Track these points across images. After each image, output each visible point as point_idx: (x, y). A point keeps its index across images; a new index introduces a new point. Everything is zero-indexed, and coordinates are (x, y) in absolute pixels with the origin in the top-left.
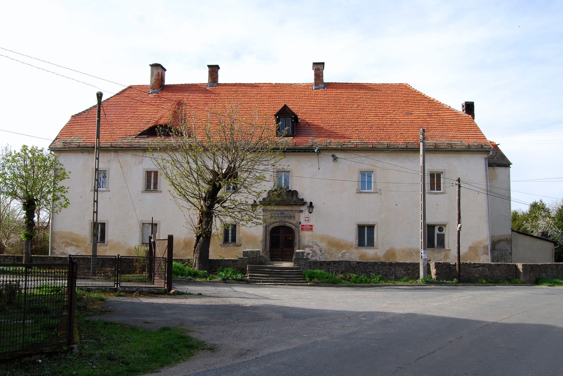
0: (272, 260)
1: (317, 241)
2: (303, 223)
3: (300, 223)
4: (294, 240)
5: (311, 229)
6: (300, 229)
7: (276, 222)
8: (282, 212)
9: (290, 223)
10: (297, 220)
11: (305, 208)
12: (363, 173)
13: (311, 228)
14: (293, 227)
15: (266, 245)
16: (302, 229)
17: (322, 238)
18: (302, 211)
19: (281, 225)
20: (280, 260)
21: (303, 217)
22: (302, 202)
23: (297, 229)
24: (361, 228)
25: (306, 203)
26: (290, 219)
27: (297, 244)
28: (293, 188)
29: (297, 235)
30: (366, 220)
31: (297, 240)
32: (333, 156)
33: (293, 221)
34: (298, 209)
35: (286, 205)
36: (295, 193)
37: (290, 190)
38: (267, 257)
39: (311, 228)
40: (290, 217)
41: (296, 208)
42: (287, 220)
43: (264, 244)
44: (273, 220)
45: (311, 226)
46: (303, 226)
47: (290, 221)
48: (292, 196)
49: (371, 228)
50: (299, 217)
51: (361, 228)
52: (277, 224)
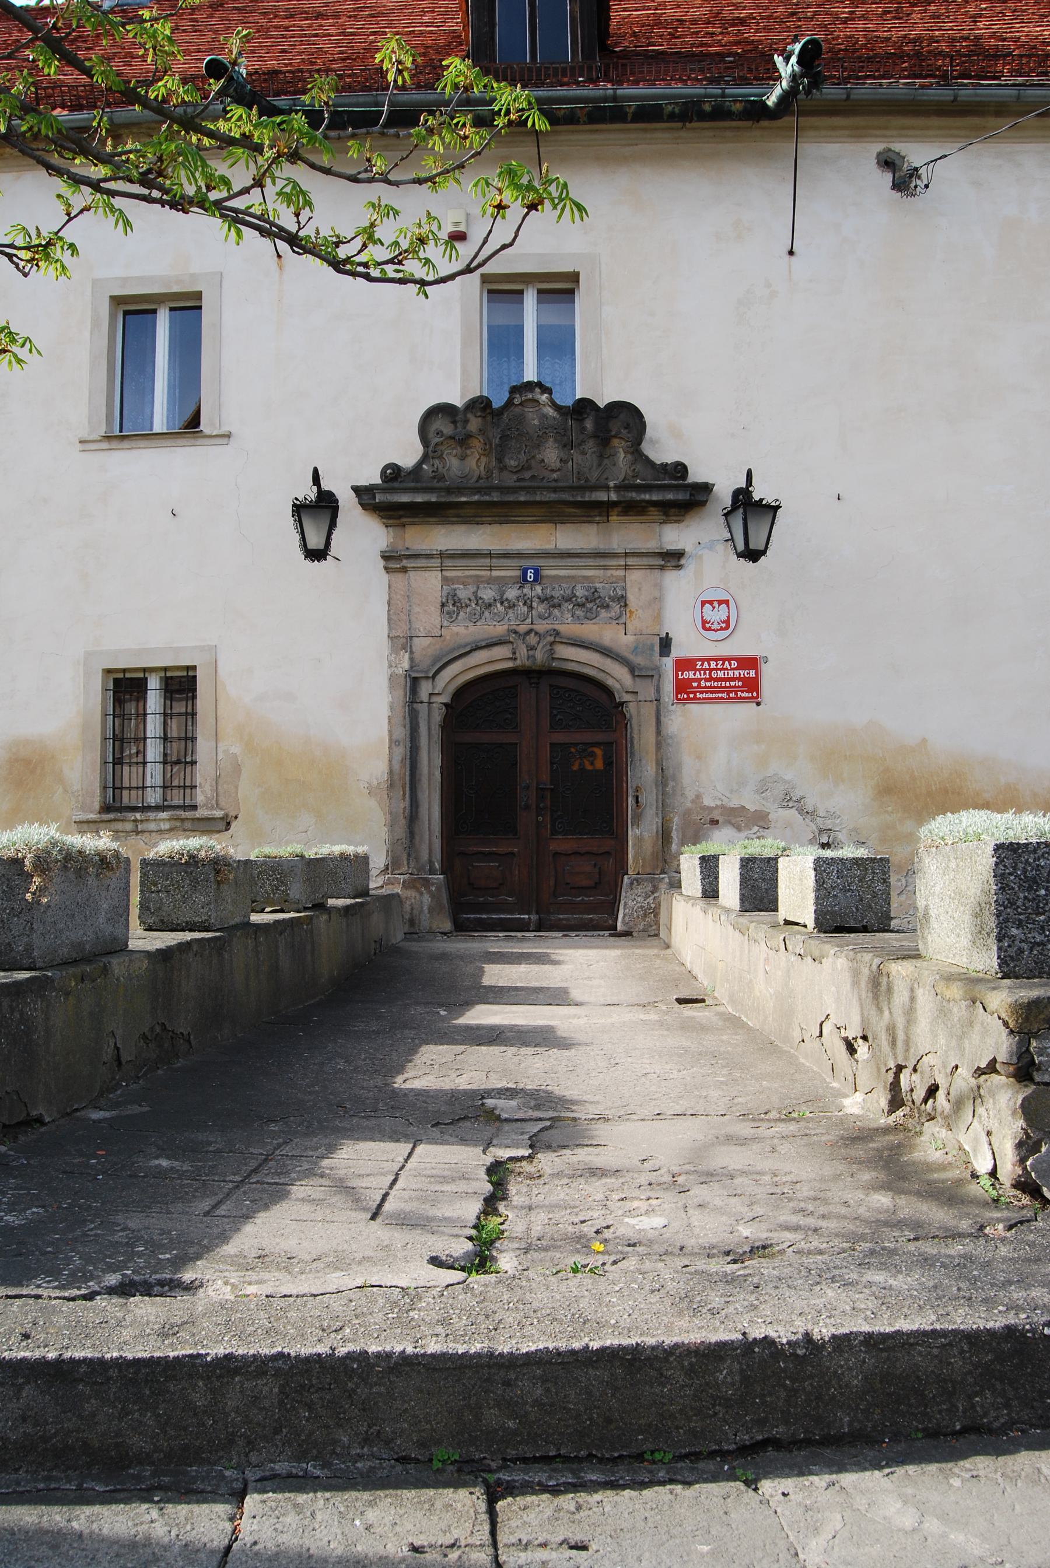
0: (461, 927)
1: (800, 775)
2: (689, 642)
3: (666, 644)
4: (622, 775)
5: (752, 686)
6: (668, 687)
7: (487, 643)
8: (530, 570)
9: (593, 645)
10: (639, 620)
11: (702, 537)
12: (133, 313)
13: (745, 680)
14: (618, 677)
15: (413, 816)
16: (682, 688)
17: (834, 755)
18: (674, 558)
19: (523, 658)
20: (522, 927)
21: (691, 597)
22: (679, 494)
23: (646, 690)
24: (125, 688)
25: (706, 488)
26: (591, 617)
27: (649, 797)
28: (598, 380)
29: (644, 737)
30: (151, 642)
31: (643, 772)
32: (888, 162)
33: (608, 634)
34: (652, 545)
35: (555, 512)
36: (625, 419)
37: (585, 405)
38: (424, 903)
39: (745, 680)
40: (593, 603)
41: (628, 535)
42: (569, 627)
43: (402, 805)
44: (463, 631)
45: (750, 663)
46: (683, 664)
47: (589, 630)
48: (604, 440)
49: (181, 685)
50: (658, 601)
51: (125, 688)
52: (498, 659)
